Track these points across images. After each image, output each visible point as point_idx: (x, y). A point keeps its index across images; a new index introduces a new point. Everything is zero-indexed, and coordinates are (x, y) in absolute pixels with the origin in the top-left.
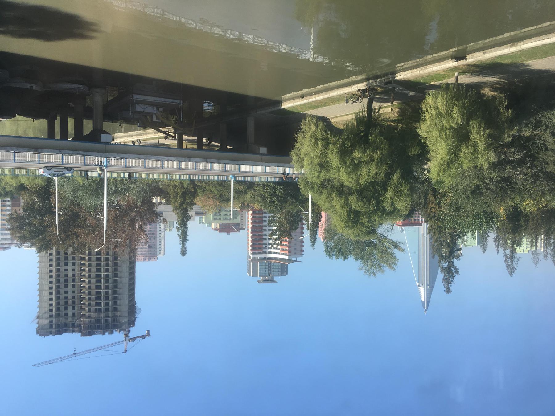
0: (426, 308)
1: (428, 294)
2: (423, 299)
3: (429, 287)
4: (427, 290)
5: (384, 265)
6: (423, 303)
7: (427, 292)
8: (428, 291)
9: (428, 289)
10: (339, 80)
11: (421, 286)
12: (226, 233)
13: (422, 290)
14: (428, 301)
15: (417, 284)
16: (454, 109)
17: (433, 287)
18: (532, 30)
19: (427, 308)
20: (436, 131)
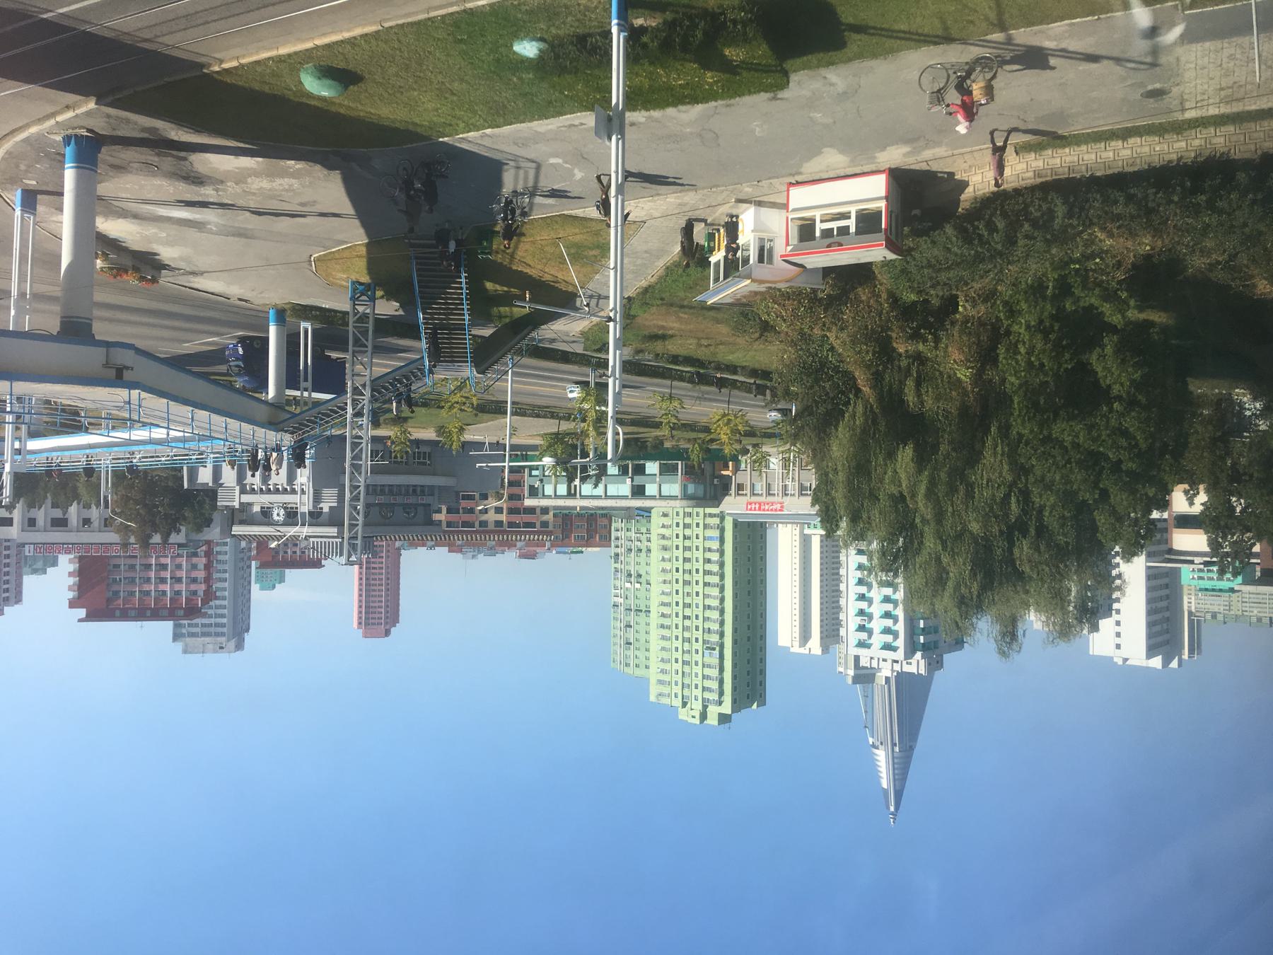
0: (892, 809)
1: (897, 763)
2: (884, 784)
3: (897, 749)
4: (893, 758)
5: (1175, 90)
6: (886, 792)
7: (894, 769)
8: (896, 777)
9: (895, 755)
10: (340, 113)
11: (877, 748)
12: (727, 497)
13: (882, 757)
14: (897, 788)
15: (871, 740)
16: (947, 230)
17: (912, 748)
18: (1260, 68)
19: (897, 807)
20: (744, 337)
